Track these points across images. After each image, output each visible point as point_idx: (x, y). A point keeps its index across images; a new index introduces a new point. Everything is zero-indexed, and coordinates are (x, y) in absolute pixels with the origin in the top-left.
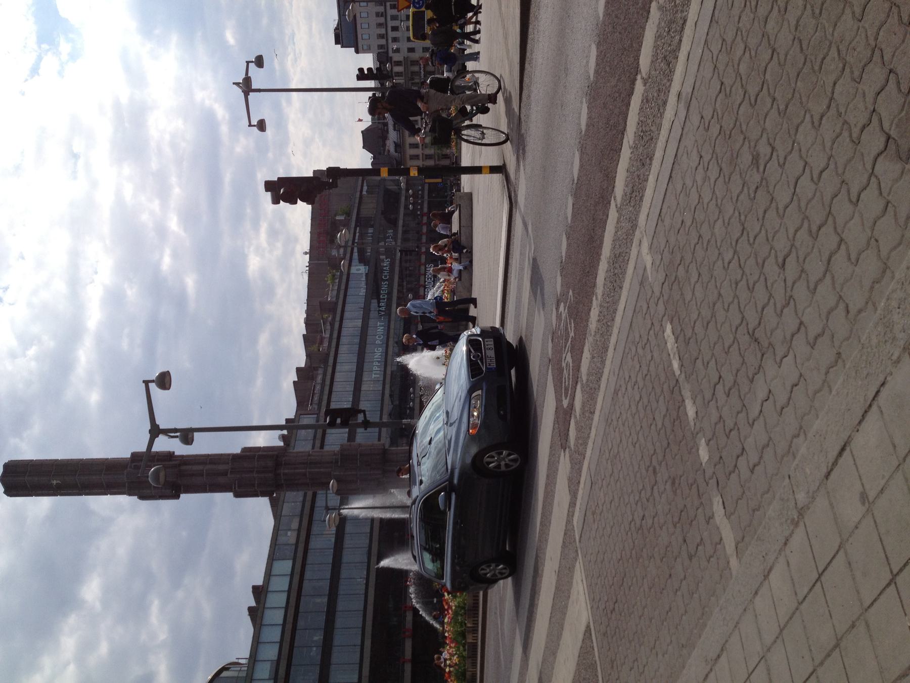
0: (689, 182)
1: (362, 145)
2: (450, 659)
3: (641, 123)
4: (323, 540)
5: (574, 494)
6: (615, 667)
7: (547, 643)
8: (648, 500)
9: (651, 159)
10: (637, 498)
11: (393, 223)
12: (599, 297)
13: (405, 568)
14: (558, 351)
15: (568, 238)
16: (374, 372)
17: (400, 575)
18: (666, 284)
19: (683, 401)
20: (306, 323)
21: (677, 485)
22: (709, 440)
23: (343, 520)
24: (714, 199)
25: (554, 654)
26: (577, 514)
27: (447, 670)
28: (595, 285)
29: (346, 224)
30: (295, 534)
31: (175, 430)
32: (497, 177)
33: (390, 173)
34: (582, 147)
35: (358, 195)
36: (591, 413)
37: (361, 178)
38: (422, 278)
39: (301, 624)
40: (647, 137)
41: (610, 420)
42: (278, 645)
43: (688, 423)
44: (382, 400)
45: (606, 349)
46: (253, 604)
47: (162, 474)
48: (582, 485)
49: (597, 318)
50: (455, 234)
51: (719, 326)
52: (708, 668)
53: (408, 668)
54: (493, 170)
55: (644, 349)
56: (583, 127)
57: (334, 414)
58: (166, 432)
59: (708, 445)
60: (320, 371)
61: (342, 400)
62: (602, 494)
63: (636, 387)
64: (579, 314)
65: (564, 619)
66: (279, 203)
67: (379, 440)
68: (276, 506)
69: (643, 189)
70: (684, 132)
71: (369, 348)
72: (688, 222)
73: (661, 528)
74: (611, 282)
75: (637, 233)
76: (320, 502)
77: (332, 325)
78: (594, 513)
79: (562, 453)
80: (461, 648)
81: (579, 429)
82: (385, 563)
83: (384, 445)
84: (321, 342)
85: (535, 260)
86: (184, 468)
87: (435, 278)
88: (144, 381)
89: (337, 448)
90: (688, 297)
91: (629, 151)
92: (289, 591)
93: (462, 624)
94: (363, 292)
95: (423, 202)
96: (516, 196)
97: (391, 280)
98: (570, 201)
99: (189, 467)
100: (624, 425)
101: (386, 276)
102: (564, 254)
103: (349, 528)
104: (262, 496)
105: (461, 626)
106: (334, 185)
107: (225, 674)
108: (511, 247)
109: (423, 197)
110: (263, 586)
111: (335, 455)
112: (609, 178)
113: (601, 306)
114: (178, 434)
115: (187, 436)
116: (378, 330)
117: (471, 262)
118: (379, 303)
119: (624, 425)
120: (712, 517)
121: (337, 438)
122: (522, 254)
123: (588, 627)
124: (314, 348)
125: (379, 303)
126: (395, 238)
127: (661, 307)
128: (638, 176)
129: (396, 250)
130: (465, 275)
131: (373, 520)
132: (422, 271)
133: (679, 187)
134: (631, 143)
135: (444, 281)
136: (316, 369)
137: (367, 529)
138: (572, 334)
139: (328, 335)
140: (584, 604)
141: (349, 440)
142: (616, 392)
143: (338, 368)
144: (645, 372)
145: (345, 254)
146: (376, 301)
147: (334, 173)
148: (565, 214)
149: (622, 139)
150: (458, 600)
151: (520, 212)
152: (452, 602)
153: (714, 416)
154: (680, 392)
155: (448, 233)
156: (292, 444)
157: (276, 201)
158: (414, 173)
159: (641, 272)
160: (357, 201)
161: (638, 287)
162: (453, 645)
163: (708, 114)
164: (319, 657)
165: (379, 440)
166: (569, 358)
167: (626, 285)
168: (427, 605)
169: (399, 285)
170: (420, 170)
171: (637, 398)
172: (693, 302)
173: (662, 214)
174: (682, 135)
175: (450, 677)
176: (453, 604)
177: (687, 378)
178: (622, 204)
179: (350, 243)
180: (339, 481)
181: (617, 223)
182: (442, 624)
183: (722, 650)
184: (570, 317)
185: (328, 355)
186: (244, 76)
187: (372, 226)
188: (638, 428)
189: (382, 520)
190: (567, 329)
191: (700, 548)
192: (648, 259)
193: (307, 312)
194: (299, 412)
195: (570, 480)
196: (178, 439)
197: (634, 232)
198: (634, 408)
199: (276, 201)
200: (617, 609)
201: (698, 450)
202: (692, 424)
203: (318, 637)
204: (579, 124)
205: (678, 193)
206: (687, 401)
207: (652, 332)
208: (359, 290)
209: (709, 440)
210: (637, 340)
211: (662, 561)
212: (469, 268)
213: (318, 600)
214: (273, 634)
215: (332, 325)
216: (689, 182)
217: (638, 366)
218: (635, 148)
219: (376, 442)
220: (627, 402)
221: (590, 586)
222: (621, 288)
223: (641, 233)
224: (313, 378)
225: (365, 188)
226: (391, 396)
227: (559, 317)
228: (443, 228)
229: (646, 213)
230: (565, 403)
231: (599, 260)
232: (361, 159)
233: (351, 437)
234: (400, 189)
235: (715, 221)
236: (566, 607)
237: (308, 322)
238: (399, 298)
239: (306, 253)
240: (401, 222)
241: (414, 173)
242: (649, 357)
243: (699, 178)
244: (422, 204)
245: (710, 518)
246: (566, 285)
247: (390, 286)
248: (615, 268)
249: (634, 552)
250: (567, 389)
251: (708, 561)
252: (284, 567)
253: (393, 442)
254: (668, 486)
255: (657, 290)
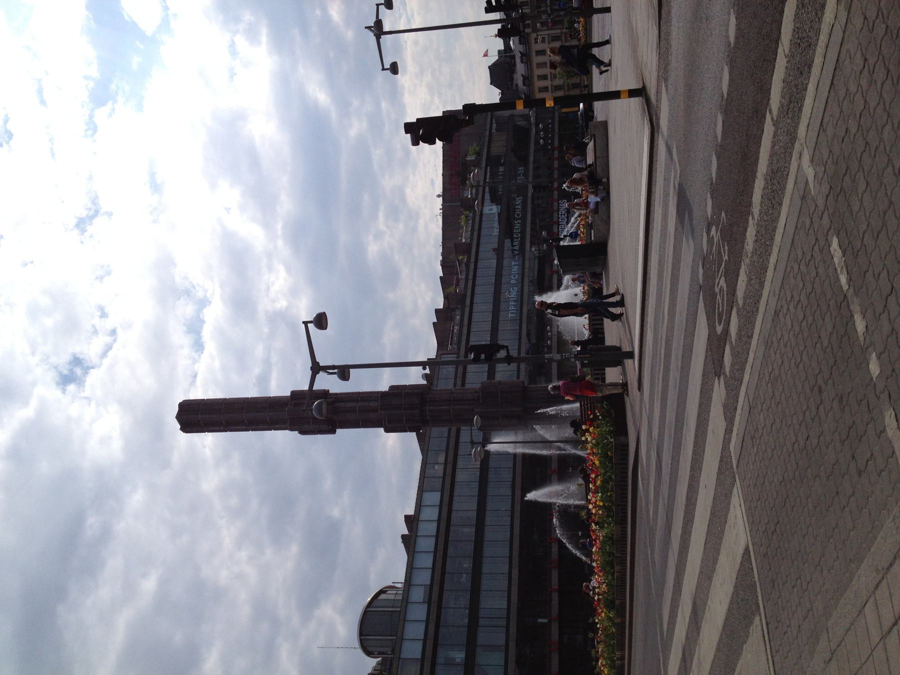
0: (853, 88)
1: (489, 81)
2: (599, 587)
3: (796, 30)
4: (468, 473)
5: (730, 421)
6: (776, 586)
7: (702, 568)
8: (813, 420)
9: (810, 67)
10: (801, 418)
11: (524, 160)
12: (756, 217)
13: (549, 501)
14: (710, 277)
15: (718, 158)
16: (510, 311)
17: (544, 509)
18: (831, 196)
19: (852, 316)
20: (442, 265)
21: (844, 403)
22: (881, 354)
23: (487, 453)
24: (882, 103)
25: (710, 578)
26: (733, 440)
27: (596, 598)
28: (750, 204)
29: (476, 164)
30: (442, 467)
31: (333, 367)
32: (636, 102)
33: (543, 101)
34: (731, 61)
35: (487, 133)
36: (748, 337)
37: (489, 114)
38: (555, 215)
39: (451, 551)
40: (804, 43)
41: (769, 343)
42: (430, 571)
43: (858, 338)
44: (520, 339)
45: (765, 269)
46: (406, 532)
47: (324, 406)
48: (739, 411)
49: (754, 238)
50: (590, 166)
51: (890, 234)
52: (881, 575)
53: (555, 597)
54: (632, 93)
55: (807, 266)
56: (732, 39)
57: (478, 349)
58: (325, 369)
59: (879, 358)
60: (458, 312)
61: (481, 336)
62: (762, 418)
63: (800, 306)
64: (733, 236)
65: (720, 544)
66: (418, 144)
67: (518, 377)
68: (422, 441)
69: (803, 99)
70: (846, 36)
71: (504, 287)
72: (853, 130)
73: (827, 447)
74: (769, 200)
75: (797, 145)
76: (465, 437)
77: (467, 266)
78: (753, 438)
79: (716, 381)
80: (610, 577)
81: (735, 355)
82: (531, 496)
83: (523, 382)
84: (457, 285)
85: (680, 185)
86: (337, 405)
87: (569, 213)
88: (304, 322)
89: (478, 386)
90: (856, 208)
91: (785, 60)
92: (439, 521)
93: (610, 554)
94: (496, 232)
95: (553, 136)
96: (658, 119)
97: (524, 219)
98: (720, 119)
99: (343, 404)
100: (785, 346)
101: (518, 215)
102: (714, 175)
103: (492, 464)
104: (410, 431)
105: (610, 556)
106: (470, 122)
107: (382, 596)
108: (654, 173)
109: (553, 130)
110: (414, 516)
111: (476, 392)
112: (764, 91)
113: (758, 225)
114: (336, 371)
115: (343, 372)
116: (513, 268)
117: (608, 193)
118: (512, 242)
119: (785, 346)
120: (883, 431)
121: (476, 375)
122: (667, 180)
123: (747, 550)
124: (451, 290)
125: (512, 242)
126: (526, 174)
127: (826, 221)
128: (796, 86)
129: (527, 187)
130: (602, 209)
131: (515, 455)
132: (555, 208)
133: (842, 93)
134: (787, 51)
135: (579, 216)
136: (453, 310)
137: (511, 464)
138: (726, 258)
139: (464, 277)
140: (742, 528)
141: (488, 379)
142: (777, 313)
143: (475, 308)
144: (809, 290)
145: (477, 194)
146: (509, 240)
147: (470, 109)
148: (715, 132)
149: (777, 49)
150: (606, 530)
151: (663, 136)
152: (599, 534)
153: (886, 329)
154: (848, 306)
155: (584, 166)
156: (435, 383)
157: (415, 143)
158: (550, 103)
159: (802, 186)
160: (487, 139)
161: (799, 203)
162: (601, 574)
163: (872, 13)
164: (469, 584)
165: (518, 377)
166: (722, 282)
167: (786, 202)
168: (574, 540)
169: (532, 223)
170: (556, 100)
171: (801, 317)
172: (862, 213)
173: (824, 123)
174: (843, 38)
175: (599, 604)
176: (601, 535)
177: (856, 294)
178: (779, 116)
179: (482, 183)
180: (482, 417)
181: (774, 136)
182: (589, 554)
183: (895, 558)
184: (723, 240)
185: (465, 296)
186: (375, 19)
187: (503, 165)
188: (802, 348)
189: (524, 455)
190: (720, 253)
191: (870, 463)
192: (810, 172)
193: (443, 254)
194: (440, 352)
195: (725, 406)
196: (336, 376)
197: (793, 145)
198: (797, 328)
199: (415, 143)
200: (778, 530)
201: (868, 364)
202: (862, 339)
203: (468, 565)
204: (727, 37)
205: (841, 99)
206: (856, 316)
207: (816, 248)
208: (492, 230)
209: (881, 354)
210: (800, 256)
211: (828, 479)
212: (606, 199)
213: (466, 530)
214: (426, 561)
215: (467, 266)
216: (853, 88)
217: (801, 285)
218: (790, 57)
219: (515, 379)
220: (789, 323)
221: (748, 510)
222: (780, 204)
223: (802, 145)
224: (452, 319)
225: (494, 126)
226: (528, 335)
227: (710, 240)
228: (578, 162)
229: (806, 124)
230: (719, 329)
231: (754, 177)
232: (490, 95)
233: (491, 373)
234: (530, 124)
235: (883, 127)
236: (723, 532)
237: (444, 264)
238: (532, 236)
239: (439, 196)
240: (531, 159)
241: (550, 103)
242: (813, 274)
243: (864, 82)
244: (552, 139)
245: (881, 432)
246: (717, 208)
247: (523, 225)
248: (773, 184)
249: (797, 473)
250: (720, 315)
251: (879, 475)
252: (433, 498)
253: (532, 378)
254: (835, 403)
255: (821, 203)
